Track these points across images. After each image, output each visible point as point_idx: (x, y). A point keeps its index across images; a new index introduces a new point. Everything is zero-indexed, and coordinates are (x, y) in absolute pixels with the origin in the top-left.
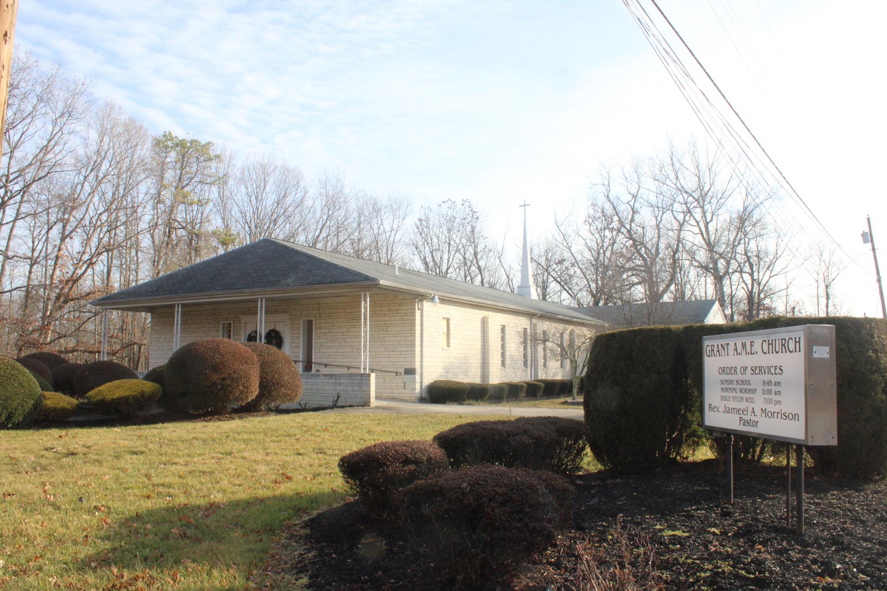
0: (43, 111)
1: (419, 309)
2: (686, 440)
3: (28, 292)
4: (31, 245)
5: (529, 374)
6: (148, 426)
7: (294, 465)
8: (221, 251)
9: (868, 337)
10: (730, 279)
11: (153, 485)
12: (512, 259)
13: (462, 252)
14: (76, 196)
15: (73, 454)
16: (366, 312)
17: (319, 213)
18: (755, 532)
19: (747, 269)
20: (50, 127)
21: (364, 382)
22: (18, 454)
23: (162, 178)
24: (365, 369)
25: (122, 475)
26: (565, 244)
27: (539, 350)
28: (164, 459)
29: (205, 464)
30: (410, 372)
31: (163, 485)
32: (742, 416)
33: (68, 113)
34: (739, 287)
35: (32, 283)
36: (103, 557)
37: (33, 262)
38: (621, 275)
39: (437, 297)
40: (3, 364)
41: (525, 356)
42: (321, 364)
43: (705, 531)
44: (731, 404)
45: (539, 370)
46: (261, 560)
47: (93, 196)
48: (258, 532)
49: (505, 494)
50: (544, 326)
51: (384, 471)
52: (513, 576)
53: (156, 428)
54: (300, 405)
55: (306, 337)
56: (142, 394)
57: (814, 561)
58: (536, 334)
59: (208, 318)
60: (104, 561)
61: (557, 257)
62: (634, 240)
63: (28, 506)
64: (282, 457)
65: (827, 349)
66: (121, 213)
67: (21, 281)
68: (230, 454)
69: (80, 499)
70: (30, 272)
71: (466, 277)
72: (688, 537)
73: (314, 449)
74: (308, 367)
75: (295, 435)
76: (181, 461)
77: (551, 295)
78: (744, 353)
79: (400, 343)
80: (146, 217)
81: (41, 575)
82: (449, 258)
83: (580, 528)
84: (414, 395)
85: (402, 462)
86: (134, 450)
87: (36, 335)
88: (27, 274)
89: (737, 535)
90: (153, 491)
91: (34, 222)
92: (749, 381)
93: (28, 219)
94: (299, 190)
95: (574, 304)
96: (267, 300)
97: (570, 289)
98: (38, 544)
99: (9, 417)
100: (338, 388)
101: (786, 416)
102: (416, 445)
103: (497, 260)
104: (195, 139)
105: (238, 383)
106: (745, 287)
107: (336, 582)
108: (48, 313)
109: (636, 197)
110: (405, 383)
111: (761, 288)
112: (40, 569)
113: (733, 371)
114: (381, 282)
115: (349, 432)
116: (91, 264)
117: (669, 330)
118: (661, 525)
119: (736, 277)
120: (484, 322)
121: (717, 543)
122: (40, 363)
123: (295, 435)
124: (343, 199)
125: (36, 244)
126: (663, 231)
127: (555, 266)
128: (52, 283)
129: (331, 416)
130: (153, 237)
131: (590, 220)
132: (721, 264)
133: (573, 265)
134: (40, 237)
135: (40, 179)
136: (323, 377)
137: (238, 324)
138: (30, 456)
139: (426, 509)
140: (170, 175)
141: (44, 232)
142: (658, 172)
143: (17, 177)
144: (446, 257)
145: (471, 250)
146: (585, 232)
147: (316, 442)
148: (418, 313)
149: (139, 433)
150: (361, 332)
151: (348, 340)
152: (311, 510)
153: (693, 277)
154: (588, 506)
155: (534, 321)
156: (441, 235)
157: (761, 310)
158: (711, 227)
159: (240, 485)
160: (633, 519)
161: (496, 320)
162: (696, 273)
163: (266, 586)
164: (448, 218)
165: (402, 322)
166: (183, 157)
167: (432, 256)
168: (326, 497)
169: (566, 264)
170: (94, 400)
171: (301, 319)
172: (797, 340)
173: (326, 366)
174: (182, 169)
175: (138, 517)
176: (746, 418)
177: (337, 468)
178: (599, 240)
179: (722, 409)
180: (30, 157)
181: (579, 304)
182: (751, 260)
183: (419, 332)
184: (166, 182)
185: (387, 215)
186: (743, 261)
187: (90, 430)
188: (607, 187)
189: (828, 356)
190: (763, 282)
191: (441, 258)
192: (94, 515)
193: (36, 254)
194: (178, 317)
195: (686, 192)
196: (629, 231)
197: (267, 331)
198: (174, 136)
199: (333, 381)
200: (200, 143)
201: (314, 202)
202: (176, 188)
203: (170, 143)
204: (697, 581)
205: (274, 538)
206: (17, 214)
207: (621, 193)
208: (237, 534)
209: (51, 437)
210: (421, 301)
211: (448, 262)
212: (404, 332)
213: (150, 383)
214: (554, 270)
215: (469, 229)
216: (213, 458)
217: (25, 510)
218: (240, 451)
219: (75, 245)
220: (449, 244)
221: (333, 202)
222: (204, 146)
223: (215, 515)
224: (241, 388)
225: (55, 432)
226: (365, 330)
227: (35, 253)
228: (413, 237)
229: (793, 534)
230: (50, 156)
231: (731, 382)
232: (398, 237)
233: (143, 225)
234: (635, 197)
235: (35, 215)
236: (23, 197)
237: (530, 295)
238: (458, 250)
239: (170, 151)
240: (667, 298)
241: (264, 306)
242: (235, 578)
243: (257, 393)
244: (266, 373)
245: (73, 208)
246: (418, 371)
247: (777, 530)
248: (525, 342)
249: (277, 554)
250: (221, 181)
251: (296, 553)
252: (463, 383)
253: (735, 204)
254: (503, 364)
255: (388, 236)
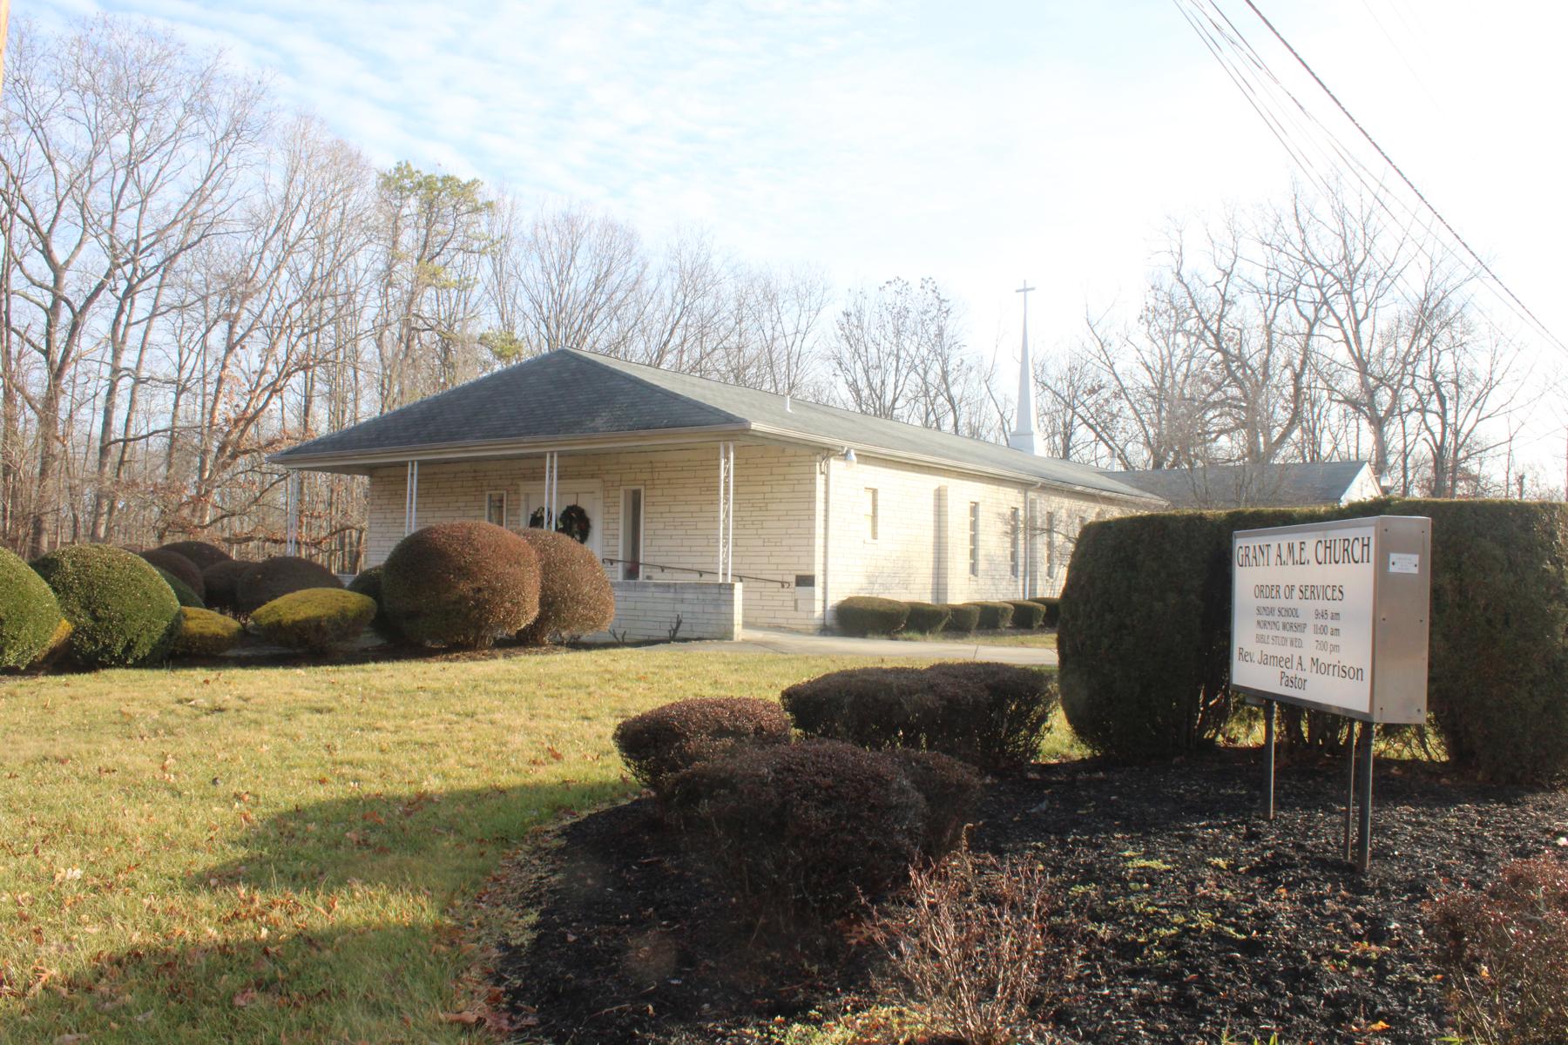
0: (194, 129)
1: (822, 473)
2: (1236, 709)
3: (173, 439)
4: (176, 358)
5: (1021, 587)
6: (353, 667)
7: (572, 735)
8: (498, 367)
9: (1546, 537)
10: (1404, 423)
11: (334, 763)
12: (1007, 384)
13: (921, 372)
14: (251, 275)
15: (221, 710)
16: (727, 477)
17: (667, 303)
18: (1285, 866)
19: (1434, 405)
20: (206, 156)
21: (723, 597)
22: (135, 709)
23: (395, 243)
24: (725, 575)
25: (290, 745)
26: (1103, 358)
27: (1039, 546)
28: (362, 721)
29: (426, 730)
30: (806, 581)
31: (351, 763)
32: (1284, 669)
33: (236, 129)
34: (1420, 438)
35: (179, 424)
36: (230, 869)
37: (181, 389)
39: (853, 452)
40: (119, 560)
41: (1014, 556)
42: (653, 566)
43: (1203, 862)
44: (1273, 650)
45: (1039, 582)
46: (475, 884)
47: (279, 274)
48: (482, 840)
49: (831, 787)
50: (1048, 504)
51: (681, 747)
52: (851, 923)
53: (363, 670)
54: (615, 635)
55: (630, 517)
56: (343, 613)
57: (1359, 917)
58: (1033, 518)
60: (230, 877)
61: (1088, 382)
62: (1225, 352)
63: (133, 789)
64: (555, 722)
65: (1415, 558)
66: (328, 303)
67: (163, 422)
68: (472, 715)
69: (214, 781)
70: (176, 406)
71: (927, 415)
72: (1169, 871)
73: (614, 710)
74: (632, 572)
75: (588, 687)
76: (390, 725)
77: (1079, 448)
78: (1290, 562)
79: (790, 531)
80: (370, 312)
81: (132, 894)
82: (897, 381)
83: (999, 852)
84: (812, 622)
85: (713, 732)
86: (319, 705)
87: (186, 512)
88: (171, 408)
89: (1252, 871)
90: (332, 773)
91: (180, 321)
92: (1296, 610)
93: (172, 315)
94: (633, 262)
95: (1118, 467)
96: (561, 455)
97: (1112, 439)
98: (138, 848)
99: (128, 648)
100: (680, 607)
101: (1345, 672)
102: (739, 706)
103: (984, 386)
104: (451, 175)
105: (503, 596)
106: (1429, 438)
107: (578, 921)
108: (207, 474)
109: (1229, 275)
110: (796, 601)
111: (1460, 440)
112: (133, 885)
113: (1274, 593)
114: (753, 426)
115: (679, 683)
116: (275, 389)
117: (1201, 518)
118: (1134, 850)
119: (1413, 420)
120: (940, 496)
121: (1212, 883)
122: (184, 558)
123: (588, 687)
124: (709, 279)
125: (185, 356)
126: (1277, 337)
127: (1085, 397)
128: (211, 423)
129: (661, 655)
130: (380, 346)
131: (1150, 315)
132: (1384, 397)
133: (1116, 396)
134: (191, 346)
135: (189, 247)
136: (653, 589)
138: (152, 712)
139: (705, 807)
140: (408, 238)
141: (198, 335)
142: (1270, 230)
143: (153, 244)
144: (891, 380)
145: (936, 368)
146: (1140, 337)
147: (620, 699)
148: (820, 480)
149: (332, 678)
150: (718, 511)
151: (700, 525)
152: (580, 809)
153: (1336, 419)
154: (1027, 815)
155: (1032, 495)
156: (883, 341)
157: (1460, 479)
158: (1365, 327)
159: (474, 767)
160: (1090, 839)
161: (961, 493)
162: (1342, 412)
163: (471, 925)
164: (895, 311)
165: (791, 495)
166: (431, 206)
167: (868, 379)
168: (609, 789)
169: (1105, 393)
170: (265, 622)
172: (1366, 542)
173: (663, 569)
174: (429, 224)
175: (298, 812)
176: (1290, 673)
177: (612, 742)
178: (1165, 352)
179: (1257, 657)
180: (175, 208)
181: (1127, 465)
182: (1443, 390)
183: (823, 513)
184: (402, 248)
185: (787, 305)
186: (1426, 392)
187: (258, 672)
188: (1177, 256)
189: (1415, 571)
190: (1465, 430)
191: (883, 383)
192: (231, 806)
193: (185, 374)
194: (412, 485)
195: (1321, 266)
196: (1216, 336)
197: (564, 508)
198: (414, 168)
199: (670, 595)
200: (458, 181)
201: (661, 287)
202: (419, 260)
203: (407, 183)
204: (1151, 941)
205: (506, 851)
206: (155, 307)
207: (1203, 270)
208: (447, 843)
209: (192, 682)
210: (826, 458)
211: (896, 388)
213: (357, 595)
214: (1083, 404)
215: (933, 329)
216: (442, 721)
217: (128, 796)
218: (488, 711)
219: (250, 358)
220: (898, 358)
221: (693, 280)
222: (465, 186)
223: (420, 812)
224: (508, 605)
225: (200, 674)
226: (726, 507)
227: (183, 372)
228: (834, 344)
229: (1348, 872)
230: (206, 206)
231: (1270, 611)
232: (807, 344)
233: (365, 324)
234: (1227, 274)
235: (183, 307)
236: (163, 277)
237: (1032, 448)
238: (913, 368)
239: (408, 196)
240: (1286, 454)
241: (555, 465)
242: (423, 909)
243: (535, 613)
244: (552, 581)
245: (245, 296)
246: (819, 580)
247: (1323, 864)
248: (1015, 530)
249: (505, 877)
250: (496, 248)
251: (534, 876)
252: (898, 603)
253: (1412, 286)
254: (974, 570)
255: (790, 344)
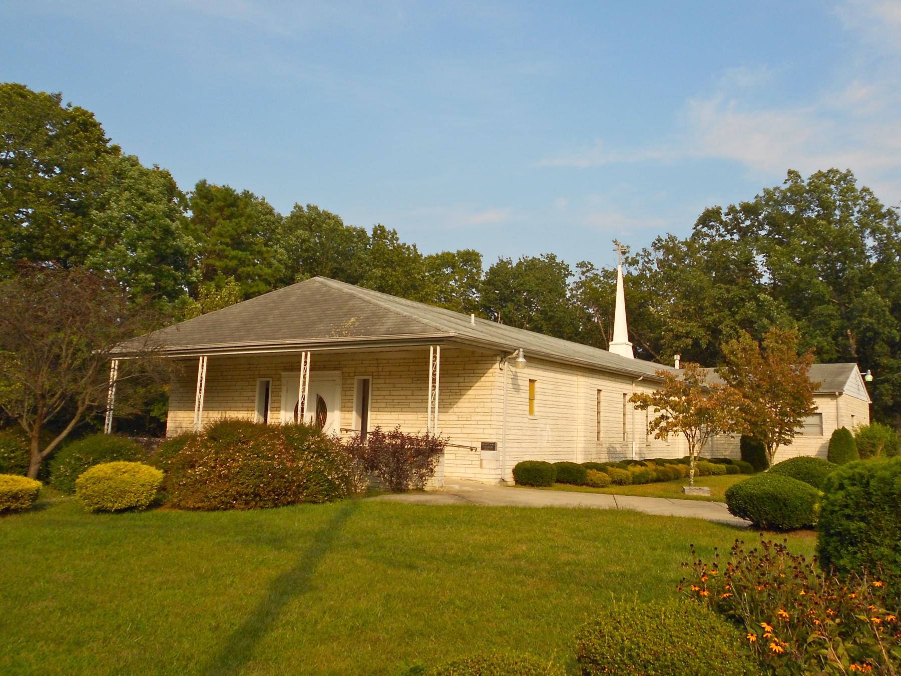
38: (274, 215)
59: (242, 373)
79: (477, 410)
137: (277, 383)
171: (356, 377)
212: (483, 397)
